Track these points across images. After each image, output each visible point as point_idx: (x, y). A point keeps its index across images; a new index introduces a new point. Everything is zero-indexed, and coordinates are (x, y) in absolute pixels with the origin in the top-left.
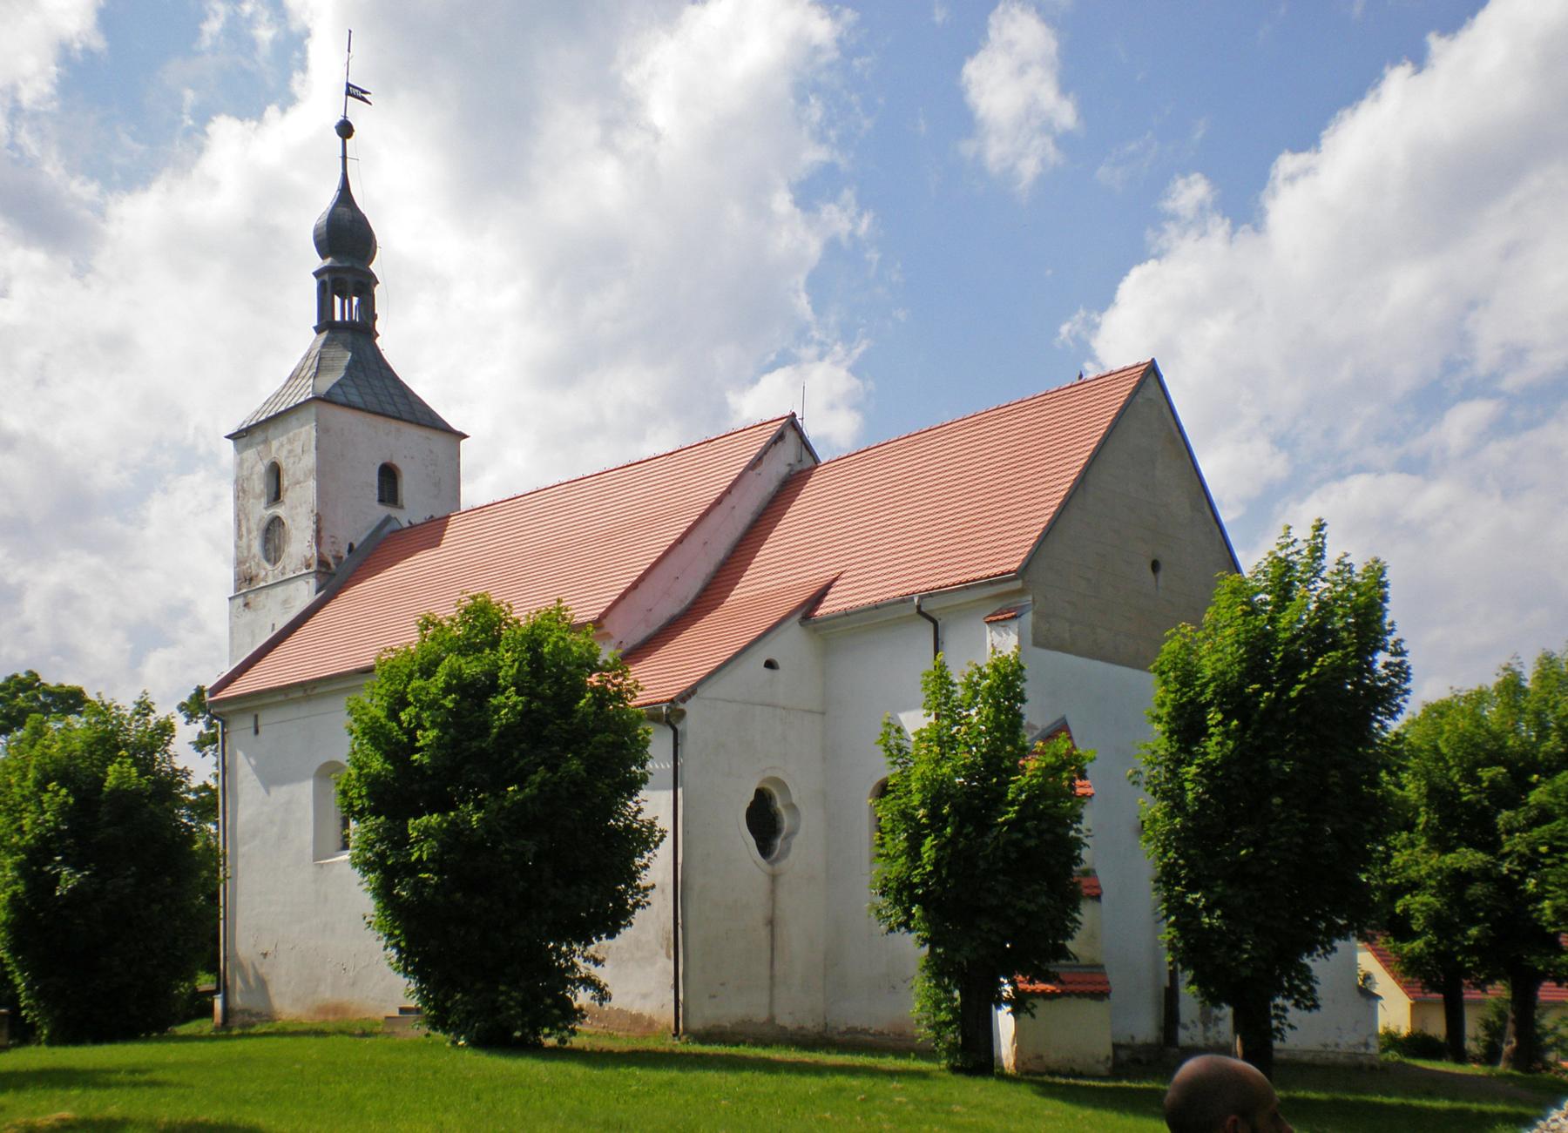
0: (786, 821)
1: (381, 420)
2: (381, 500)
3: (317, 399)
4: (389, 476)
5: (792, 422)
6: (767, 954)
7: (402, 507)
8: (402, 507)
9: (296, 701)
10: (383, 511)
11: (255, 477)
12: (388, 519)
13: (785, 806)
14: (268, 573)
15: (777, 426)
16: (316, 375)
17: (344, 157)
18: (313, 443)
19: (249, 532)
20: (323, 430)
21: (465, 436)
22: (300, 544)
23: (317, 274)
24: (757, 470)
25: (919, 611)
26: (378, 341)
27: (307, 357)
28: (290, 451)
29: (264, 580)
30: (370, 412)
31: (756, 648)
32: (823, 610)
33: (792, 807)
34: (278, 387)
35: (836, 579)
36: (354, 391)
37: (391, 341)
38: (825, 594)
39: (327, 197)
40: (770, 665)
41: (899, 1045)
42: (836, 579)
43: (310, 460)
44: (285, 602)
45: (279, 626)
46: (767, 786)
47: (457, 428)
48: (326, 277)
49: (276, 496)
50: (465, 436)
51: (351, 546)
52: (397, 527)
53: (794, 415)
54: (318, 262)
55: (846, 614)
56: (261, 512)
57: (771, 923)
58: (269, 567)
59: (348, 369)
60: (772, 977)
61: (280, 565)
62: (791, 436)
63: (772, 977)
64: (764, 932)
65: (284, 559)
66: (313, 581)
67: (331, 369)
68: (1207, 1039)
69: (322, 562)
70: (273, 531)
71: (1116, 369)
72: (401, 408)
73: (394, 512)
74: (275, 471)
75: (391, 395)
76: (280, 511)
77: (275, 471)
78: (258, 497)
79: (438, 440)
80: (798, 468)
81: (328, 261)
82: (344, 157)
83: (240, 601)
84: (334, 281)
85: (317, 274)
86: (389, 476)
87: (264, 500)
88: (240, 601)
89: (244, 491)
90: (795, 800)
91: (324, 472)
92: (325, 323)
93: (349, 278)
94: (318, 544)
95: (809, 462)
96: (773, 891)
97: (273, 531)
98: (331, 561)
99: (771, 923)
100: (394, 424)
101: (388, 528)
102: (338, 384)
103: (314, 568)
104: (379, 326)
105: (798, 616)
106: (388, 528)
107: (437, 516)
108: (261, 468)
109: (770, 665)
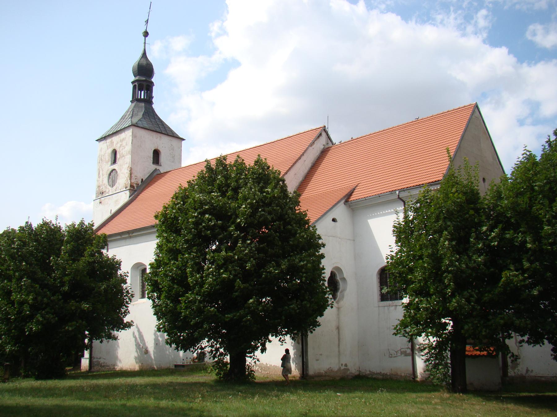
0: (341, 285)
1: (155, 133)
2: (153, 163)
3: (133, 125)
4: (156, 154)
5: (324, 129)
6: (337, 342)
7: (161, 166)
8: (161, 166)
9: (125, 239)
10: (154, 167)
11: (106, 155)
12: (156, 170)
13: (341, 279)
14: (111, 190)
15: (319, 131)
16: (132, 117)
17: (145, 43)
18: (131, 141)
19: (103, 175)
20: (134, 136)
21: (184, 140)
22: (123, 180)
23: (133, 83)
24: (313, 147)
25: (399, 198)
26: (153, 106)
27: (127, 112)
28: (121, 145)
29: (108, 193)
30: (151, 130)
31: (329, 213)
32: (352, 198)
33: (344, 279)
34: (118, 121)
35: (357, 186)
36: (145, 123)
37: (158, 106)
38: (353, 192)
39: (136, 58)
40: (334, 220)
41: (406, 383)
42: (357, 186)
43: (129, 147)
44: (116, 201)
45: (114, 211)
46: (334, 270)
47: (181, 137)
48: (136, 84)
49: (114, 162)
50: (184, 140)
51: (142, 179)
52: (159, 173)
53: (325, 127)
54: (133, 78)
55: (365, 199)
56: (109, 167)
57: (338, 328)
58: (110, 188)
59: (143, 115)
60: (339, 352)
61: (115, 187)
62: (324, 134)
63: (339, 352)
64: (336, 332)
65: (117, 185)
66: (128, 193)
67: (137, 115)
68: (515, 373)
69: (132, 186)
70: (112, 175)
71: (466, 104)
72: (162, 129)
73: (158, 167)
74: (115, 152)
75: (158, 125)
76: (115, 167)
77: (115, 152)
78: (107, 162)
79: (174, 142)
80: (327, 147)
81: (137, 78)
82: (145, 43)
83: (98, 201)
84: (139, 85)
85: (133, 83)
86: (156, 154)
87: (110, 163)
88: (98, 201)
89: (102, 160)
90: (345, 276)
91: (134, 152)
92: (135, 99)
93: (145, 84)
94: (130, 179)
95: (330, 145)
96: (338, 314)
97: (112, 175)
98: (135, 185)
99: (338, 328)
100: (159, 135)
101: (155, 174)
102: (140, 120)
103: (129, 188)
104: (153, 100)
105: (343, 201)
106: (155, 174)
107: (354, 138)
108: (110, 150)
109: (334, 220)
